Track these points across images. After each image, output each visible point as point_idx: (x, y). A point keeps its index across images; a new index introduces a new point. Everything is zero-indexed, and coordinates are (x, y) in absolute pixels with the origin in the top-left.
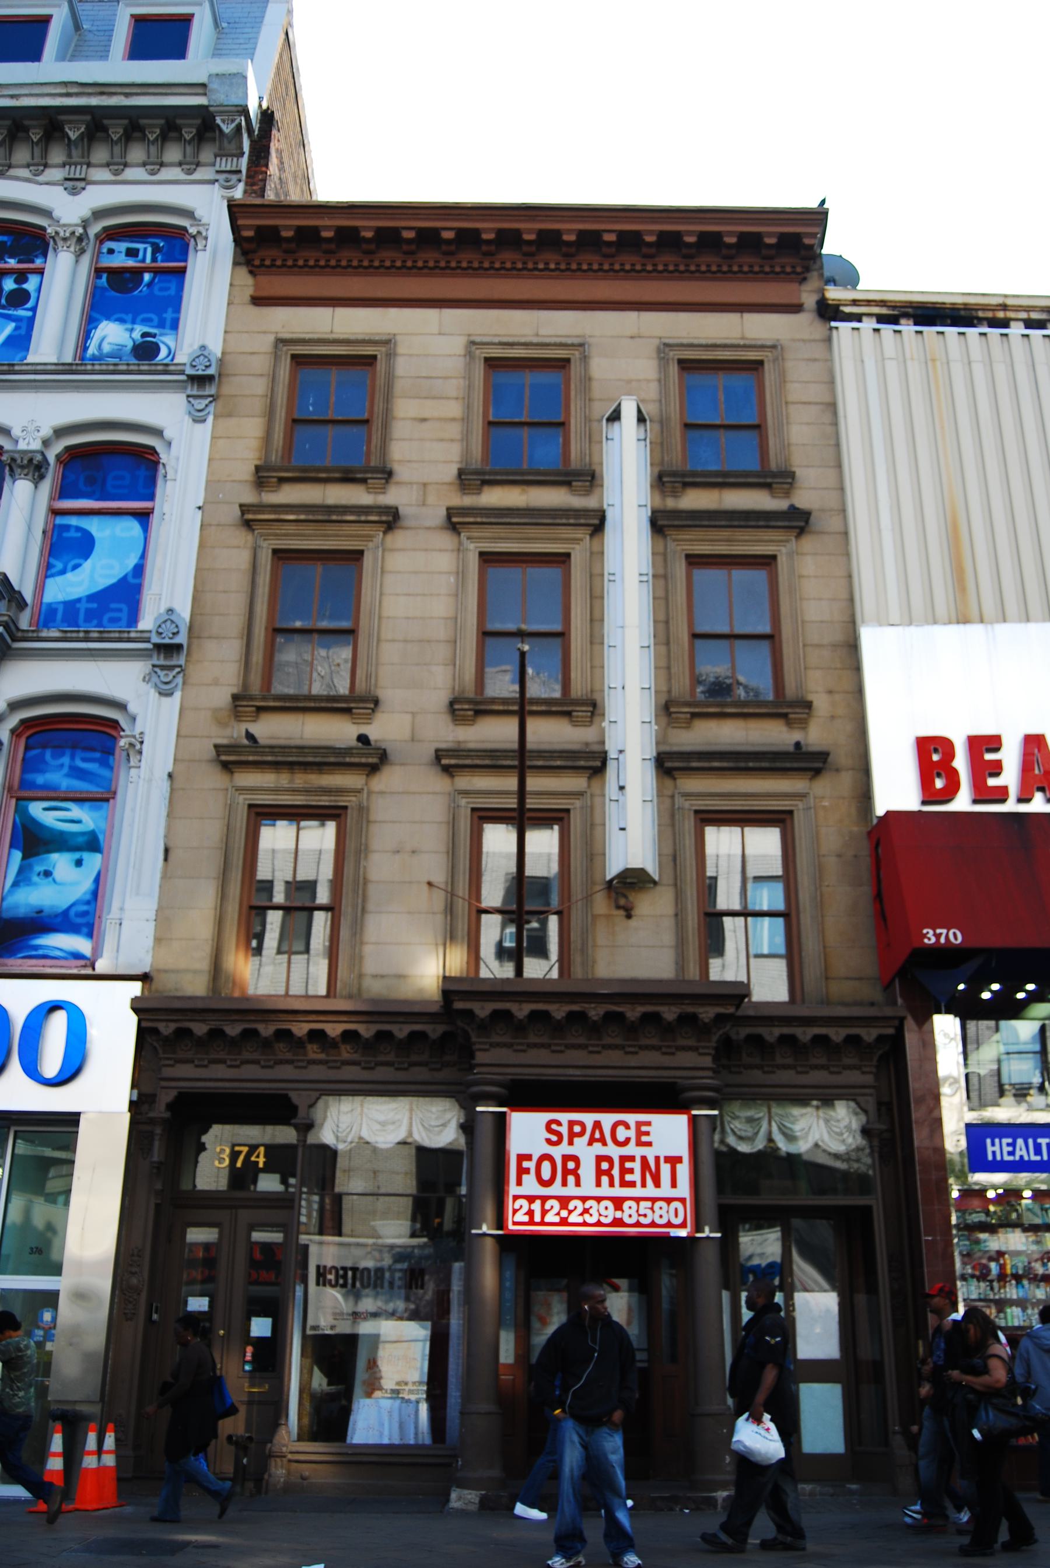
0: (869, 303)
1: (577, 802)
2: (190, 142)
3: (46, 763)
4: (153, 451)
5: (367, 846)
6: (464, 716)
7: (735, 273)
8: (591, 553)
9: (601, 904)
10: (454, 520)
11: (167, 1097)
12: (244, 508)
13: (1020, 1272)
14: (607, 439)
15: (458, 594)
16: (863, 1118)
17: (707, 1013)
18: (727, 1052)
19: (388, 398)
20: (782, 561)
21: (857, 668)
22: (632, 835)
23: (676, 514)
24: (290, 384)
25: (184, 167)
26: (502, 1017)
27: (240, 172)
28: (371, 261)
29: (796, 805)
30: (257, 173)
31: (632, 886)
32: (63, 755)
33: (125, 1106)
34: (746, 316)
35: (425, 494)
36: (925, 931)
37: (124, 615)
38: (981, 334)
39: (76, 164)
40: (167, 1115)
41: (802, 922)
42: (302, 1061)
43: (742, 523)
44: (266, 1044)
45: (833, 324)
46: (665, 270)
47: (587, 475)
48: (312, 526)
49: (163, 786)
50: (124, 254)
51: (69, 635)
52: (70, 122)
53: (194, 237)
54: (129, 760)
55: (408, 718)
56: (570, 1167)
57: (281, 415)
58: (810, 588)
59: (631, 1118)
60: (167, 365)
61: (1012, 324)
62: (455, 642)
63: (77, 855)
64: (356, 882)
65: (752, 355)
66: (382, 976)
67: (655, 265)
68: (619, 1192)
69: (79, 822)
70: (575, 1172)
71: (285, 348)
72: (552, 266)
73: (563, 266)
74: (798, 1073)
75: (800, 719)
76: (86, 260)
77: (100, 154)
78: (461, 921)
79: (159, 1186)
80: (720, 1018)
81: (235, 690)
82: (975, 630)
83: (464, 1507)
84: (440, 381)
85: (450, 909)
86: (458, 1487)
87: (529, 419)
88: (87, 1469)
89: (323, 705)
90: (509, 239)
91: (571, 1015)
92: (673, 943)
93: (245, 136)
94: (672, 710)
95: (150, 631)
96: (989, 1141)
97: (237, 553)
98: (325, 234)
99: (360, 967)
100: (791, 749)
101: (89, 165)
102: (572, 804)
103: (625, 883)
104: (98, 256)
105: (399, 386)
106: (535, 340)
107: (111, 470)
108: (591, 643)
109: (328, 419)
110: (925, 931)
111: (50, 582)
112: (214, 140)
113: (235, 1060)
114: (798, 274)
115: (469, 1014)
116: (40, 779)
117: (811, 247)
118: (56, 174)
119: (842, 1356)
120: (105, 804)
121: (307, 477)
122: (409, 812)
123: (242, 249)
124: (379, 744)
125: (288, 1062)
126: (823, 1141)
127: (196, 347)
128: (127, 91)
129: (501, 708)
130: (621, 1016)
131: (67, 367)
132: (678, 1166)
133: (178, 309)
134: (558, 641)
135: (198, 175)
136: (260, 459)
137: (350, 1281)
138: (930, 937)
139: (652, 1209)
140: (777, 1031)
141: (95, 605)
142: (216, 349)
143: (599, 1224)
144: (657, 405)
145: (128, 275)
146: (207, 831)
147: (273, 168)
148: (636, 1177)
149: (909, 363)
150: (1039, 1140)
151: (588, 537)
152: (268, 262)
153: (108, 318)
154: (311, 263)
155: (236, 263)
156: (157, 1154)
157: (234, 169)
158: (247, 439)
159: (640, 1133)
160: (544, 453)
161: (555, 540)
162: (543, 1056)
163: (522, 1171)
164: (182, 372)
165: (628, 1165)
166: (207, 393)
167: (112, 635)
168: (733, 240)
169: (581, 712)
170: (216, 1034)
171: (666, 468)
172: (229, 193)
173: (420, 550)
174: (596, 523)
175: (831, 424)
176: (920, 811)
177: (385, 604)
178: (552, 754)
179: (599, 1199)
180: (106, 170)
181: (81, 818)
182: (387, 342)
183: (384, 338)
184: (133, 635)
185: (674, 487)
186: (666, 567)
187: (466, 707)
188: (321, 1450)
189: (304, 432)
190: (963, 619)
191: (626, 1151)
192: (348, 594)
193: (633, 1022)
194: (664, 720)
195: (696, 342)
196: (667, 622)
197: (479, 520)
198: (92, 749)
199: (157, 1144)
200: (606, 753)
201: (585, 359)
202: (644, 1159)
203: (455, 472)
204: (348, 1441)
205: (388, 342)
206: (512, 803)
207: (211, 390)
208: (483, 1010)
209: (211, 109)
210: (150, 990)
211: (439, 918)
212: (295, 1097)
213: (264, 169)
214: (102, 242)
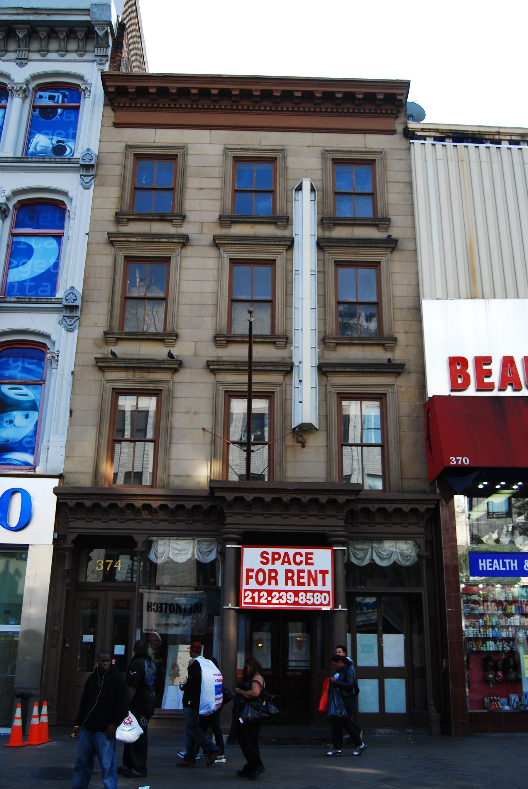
0: (430, 130)
3: (9, 365)
4: (63, 203)
5: (172, 411)
6: (221, 343)
8: (287, 260)
9: (290, 440)
10: (217, 242)
11: (72, 537)
12: (110, 235)
13: (494, 624)
14: (295, 200)
15: (218, 280)
16: (418, 550)
17: (342, 499)
18: (352, 517)
19: (183, 177)
20: (383, 265)
21: (420, 321)
22: (305, 403)
23: (330, 240)
24: (133, 169)
25: (78, 53)
27: (107, 56)
29: (388, 391)
30: (116, 56)
31: (305, 431)
32: (18, 361)
33: (51, 543)
34: (367, 136)
35: (202, 227)
36: (451, 458)
37: (49, 289)
38: (486, 147)
39: (22, 51)
40: (72, 546)
41: (390, 450)
42: (139, 519)
43: (363, 245)
44: (122, 511)
45: (411, 141)
46: (326, 111)
47: (285, 219)
48: (144, 244)
50: (47, 98)
51: (20, 300)
52: (19, 28)
53: (84, 90)
54: (51, 364)
55: (193, 343)
56: (273, 576)
58: (397, 278)
59: (303, 551)
60: (70, 159)
61: (503, 142)
62: (217, 305)
63: (26, 412)
64: (166, 428)
66: (179, 476)
67: (321, 108)
68: (297, 588)
69: (27, 395)
70: (275, 578)
71: (130, 150)
72: (268, 108)
74: (386, 526)
76: (28, 102)
77: (35, 46)
78: (219, 450)
79: (68, 581)
80: (348, 501)
81: (105, 330)
82: (479, 302)
84: (210, 168)
85: (213, 442)
87: (256, 187)
88: (33, 725)
89: (150, 337)
90: (246, 94)
91: (274, 499)
92: (325, 460)
93: (110, 37)
94: (326, 341)
95: (62, 298)
96: (480, 561)
97: (106, 258)
98: (151, 91)
99: (169, 472)
100: (386, 362)
101: (29, 51)
102: (276, 389)
103: (302, 430)
104: (34, 99)
106: (259, 147)
107: (42, 213)
108: (286, 306)
109: (151, 190)
110: (451, 458)
111: (10, 270)
112: (94, 38)
113: (106, 519)
114: (394, 114)
115: (223, 498)
116: (7, 373)
117: (401, 100)
118: (12, 56)
120: (40, 386)
122: (193, 395)
123: (108, 97)
124: (178, 358)
125: (132, 520)
126: (398, 560)
127: (85, 149)
128: (49, 12)
129: (240, 339)
130: (299, 500)
131: (19, 160)
132: (326, 575)
133: (75, 128)
134: (271, 195)
135: (85, 58)
136: (118, 209)
137: (164, 610)
138: (453, 461)
139: (313, 596)
140: (376, 506)
141: (34, 284)
142: (95, 150)
143: (287, 604)
144: (321, 182)
145: (50, 110)
146: (91, 401)
147: (125, 54)
148: (305, 580)
149: (449, 162)
150: (505, 560)
151: (285, 251)
152: (122, 105)
153: (40, 133)
154: (144, 105)
155: (105, 105)
156: (67, 566)
157: (104, 54)
158: (111, 198)
159: (307, 559)
160: (262, 206)
162: (260, 520)
163: (249, 577)
164: (78, 163)
165: (301, 574)
166: (90, 174)
167: (43, 300)
168: (361, 96)
170: (96, 506)
171: (325, 216)
172: (101, 67)
173: (199, 257)
174: (289, 244)
175: (409, 193)
177: (181, 285)
178: (265, 364)
179: (287, 592)
180: (38, 54)
181: (27, 393)
182: (183, 148)
183: (182, 145)
184: (53, 300)
185: (329, 226)
186: (324, 267)
187: (223, 339)
189: (139, 193)
190: (473, 297)
191: (301, 567)
192: (164, 281)
193: (304, 503)
194: (322, 346)
195: (341, 149)
196: (324, 296)
197: (229, 242)
198: (33, 358)
199: (67, 560)
200: (293, 363)
201: (284, 157)
202: (309, 571)
203: (217, 216)
204: (162, 708)
205: (183, 148)
206: (245, 388)
207: (93, 172)
208: (230, 497)
209: (92, 23)
210: (63, 483)
211: (208, 447)
212: (136, 538)
213: (120, 54)
214: (36, 92)
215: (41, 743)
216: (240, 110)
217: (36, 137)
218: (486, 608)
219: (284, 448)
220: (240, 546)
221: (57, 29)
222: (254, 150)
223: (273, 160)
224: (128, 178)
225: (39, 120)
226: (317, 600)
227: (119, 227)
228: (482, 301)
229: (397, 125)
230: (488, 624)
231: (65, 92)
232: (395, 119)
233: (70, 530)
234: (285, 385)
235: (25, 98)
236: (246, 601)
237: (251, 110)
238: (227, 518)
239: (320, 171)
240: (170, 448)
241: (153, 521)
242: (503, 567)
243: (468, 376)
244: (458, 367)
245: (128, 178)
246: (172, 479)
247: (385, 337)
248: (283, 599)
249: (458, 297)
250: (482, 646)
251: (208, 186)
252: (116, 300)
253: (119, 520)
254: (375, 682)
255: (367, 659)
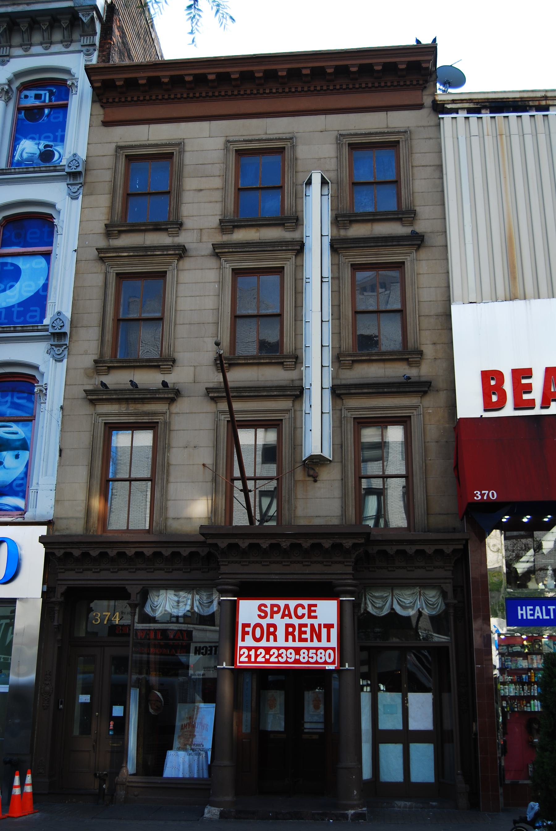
0: (462, 101)
1: (286, 415)
2: (66, 28)
7: (383, 87)
8: (296, 266)
9: (300, 474)
11: (61, 589)
12: (99, 250)
15: (220, 295)
17: (348, 543)
19: (180, 178)
20: (408, 265)
22: (317, 434)
26: (233, 547)
27: (95, 45)
28: (169, 95)
31: (316, 464)
32: (7, 396)
33: (40, 595)
34: (390, 113)
36: (475, 492)
37: (38, 314)
40: (61, 599)
43: (383, 244)
45: (440, 116)
47: (294, 219)
49: (57, 414)
50: (33, 98)
51: (5, 329)
53: (70, 86)
55: (192, 368)
57: (120, 192)
58: (424, 281)
59: (305, 603)
63: (16, 452)
64: (163, 465)
65: (393, 138)
67: (335, 86)
68: (298, 644)
69: (17, 433)
70: (274, 634)
71: (121, 152)
72: (274, 91)
73: (280, 91)
75: (416, 361)
79: (59, 637)
80: (355, 545)
81: (96, 357)
82: (519, 304)
83: (211, 817)
85: (215, 480)
86: (210, 805)
87: (261, 188)
89: (144, 364)
94: (341, 359)
96: (519, 608)
97: (96, 278)
98: (141, 82)
101: (11, 47)
104: (19, 100)
105: (187, 170)
106: (264, 137)
107: (33, 228)
108: (295, 320)
109: (144, 193)
110: (475, 492)
114: (421, 85)
115: (216, 545)
119: (434, 728)
120: (30, 423)
121: (134, 229)
122: (194, 426)
129: (243, 362)
133: (64, 130)
135: (71, 48)
136: (108, 220)
137: (213, 652)
139: (316, 654)
140: (395, 548)
141: (22, 309)
142: (83, 155)
143: (287, 662)
144: (336, 172)
145: (36, 111)
146: (82, 439)
148: (308, 636)
149: (486, 137)
150: (549, 607)
151: (294, 256)
152: (110, 100)
155: (93, 101)
157: (91, 43)
159: (310, 611)
160: (269, 205)
161: (276, 259)
163: (245, 633)
164: (63, 170)
165: (303, 629)
166: (78, 182)
167: (29, 328)
168: (380, 68)
169: (289, 362)
170: (86, 555)
174: (299, 248)
176: (481, 419)
179: (287, 649)
181: (17, 431)
182: (179, 144)
184: (40, 328)
185: (344, 224)
188: (144, 780)
190: (512, 297)
194: (337, 365)
195: (359, 132)
196: (339, 306)
197: (231, 250)
198: (23, 392)
199: (56, 615)
201: (293, 147)
202: (312, 626)
205: (180, 144)
207: (82, 180)
209: (76, 8)
211: (209, 484)
212: (129, 589)
213: (109, 41)
215: (22, 814)
216: (242, 95)
217: (22, 142)
218: (530, 661)
219: (292, 484)
220: (236, 598)
221: (39, 19)
222: (259, 140)
223: (281, 150)
224: (119, 184)
225: (25, 123)
226: (321, 658)
227: (110, 240)
228: (523, 302)
229: (425, 98)
230: (533, 680)
231: (52, 88)
232: (422, 91)
233: (59, 582)
234: (295, 411)
235: (7, 102)
236: (242, 659)
237: (255, 94)
238: (222, 567)
239: (335, 159)
240: (167, 487)
241: (148, 570)
242: (546, 615)
243: (504, 392)
244: (493, 383)
245: (119, 184)
246: (170, 522)
247: (409, 350)
248: (282, 658)
249: (494, 299)
250: (526, 706)
251: (207, 187)
252: (107, 324)
253: (111, 570)
254: (399, 747)
255: (390, 721)
